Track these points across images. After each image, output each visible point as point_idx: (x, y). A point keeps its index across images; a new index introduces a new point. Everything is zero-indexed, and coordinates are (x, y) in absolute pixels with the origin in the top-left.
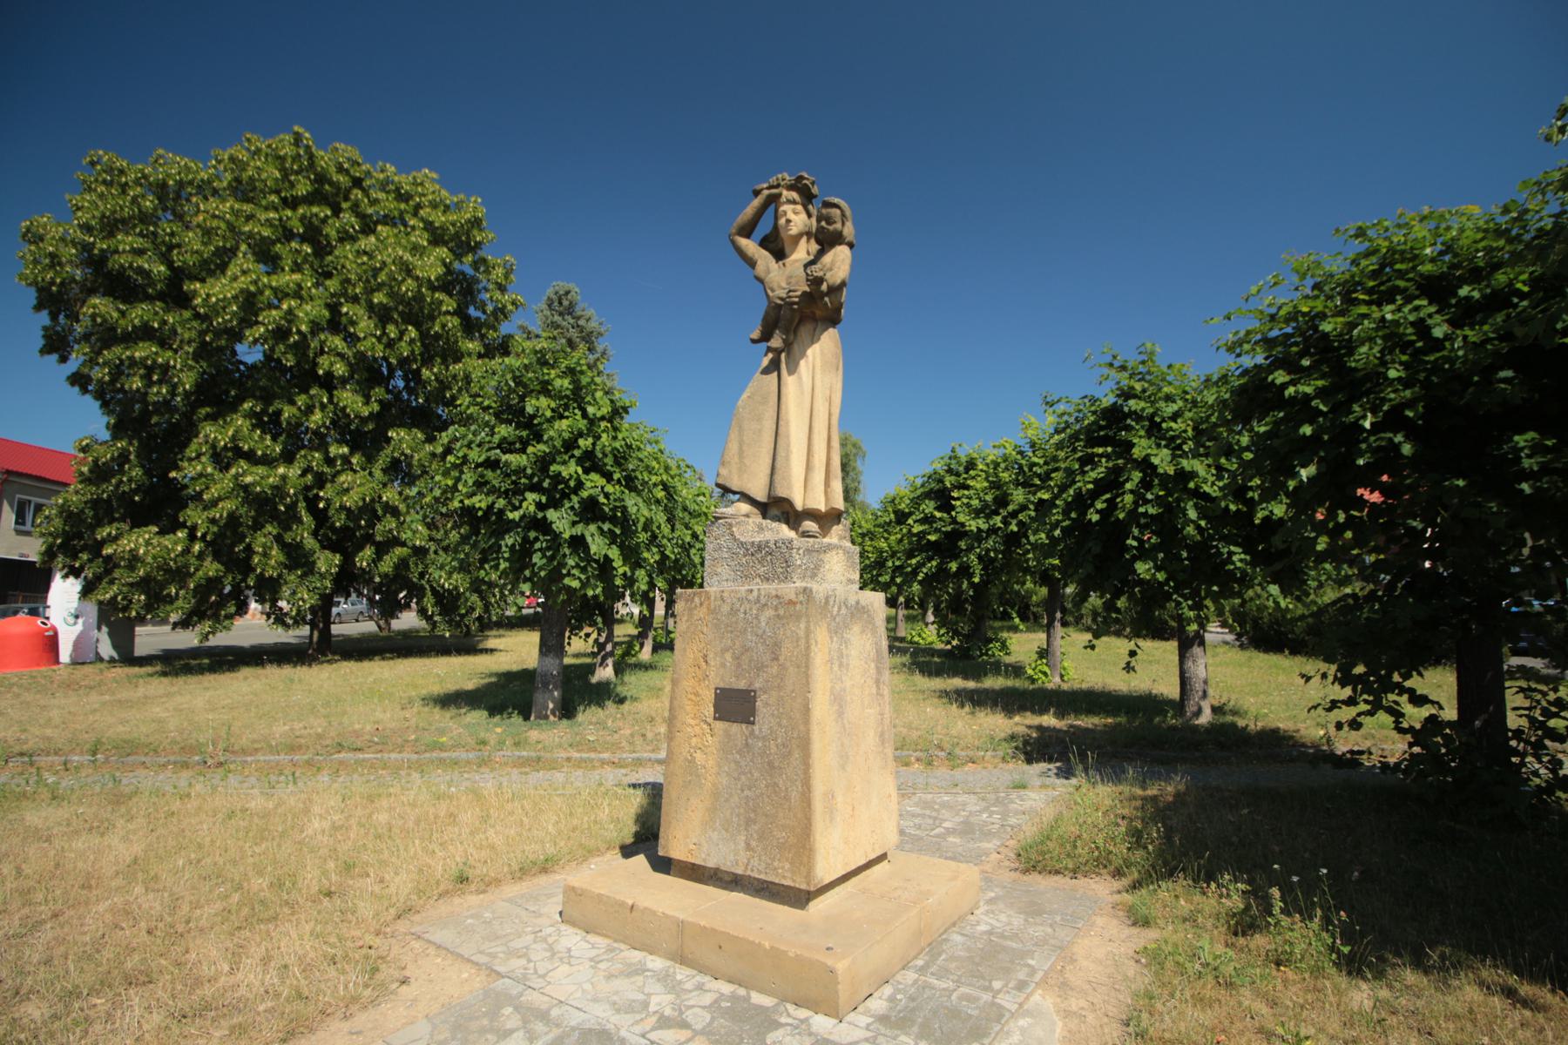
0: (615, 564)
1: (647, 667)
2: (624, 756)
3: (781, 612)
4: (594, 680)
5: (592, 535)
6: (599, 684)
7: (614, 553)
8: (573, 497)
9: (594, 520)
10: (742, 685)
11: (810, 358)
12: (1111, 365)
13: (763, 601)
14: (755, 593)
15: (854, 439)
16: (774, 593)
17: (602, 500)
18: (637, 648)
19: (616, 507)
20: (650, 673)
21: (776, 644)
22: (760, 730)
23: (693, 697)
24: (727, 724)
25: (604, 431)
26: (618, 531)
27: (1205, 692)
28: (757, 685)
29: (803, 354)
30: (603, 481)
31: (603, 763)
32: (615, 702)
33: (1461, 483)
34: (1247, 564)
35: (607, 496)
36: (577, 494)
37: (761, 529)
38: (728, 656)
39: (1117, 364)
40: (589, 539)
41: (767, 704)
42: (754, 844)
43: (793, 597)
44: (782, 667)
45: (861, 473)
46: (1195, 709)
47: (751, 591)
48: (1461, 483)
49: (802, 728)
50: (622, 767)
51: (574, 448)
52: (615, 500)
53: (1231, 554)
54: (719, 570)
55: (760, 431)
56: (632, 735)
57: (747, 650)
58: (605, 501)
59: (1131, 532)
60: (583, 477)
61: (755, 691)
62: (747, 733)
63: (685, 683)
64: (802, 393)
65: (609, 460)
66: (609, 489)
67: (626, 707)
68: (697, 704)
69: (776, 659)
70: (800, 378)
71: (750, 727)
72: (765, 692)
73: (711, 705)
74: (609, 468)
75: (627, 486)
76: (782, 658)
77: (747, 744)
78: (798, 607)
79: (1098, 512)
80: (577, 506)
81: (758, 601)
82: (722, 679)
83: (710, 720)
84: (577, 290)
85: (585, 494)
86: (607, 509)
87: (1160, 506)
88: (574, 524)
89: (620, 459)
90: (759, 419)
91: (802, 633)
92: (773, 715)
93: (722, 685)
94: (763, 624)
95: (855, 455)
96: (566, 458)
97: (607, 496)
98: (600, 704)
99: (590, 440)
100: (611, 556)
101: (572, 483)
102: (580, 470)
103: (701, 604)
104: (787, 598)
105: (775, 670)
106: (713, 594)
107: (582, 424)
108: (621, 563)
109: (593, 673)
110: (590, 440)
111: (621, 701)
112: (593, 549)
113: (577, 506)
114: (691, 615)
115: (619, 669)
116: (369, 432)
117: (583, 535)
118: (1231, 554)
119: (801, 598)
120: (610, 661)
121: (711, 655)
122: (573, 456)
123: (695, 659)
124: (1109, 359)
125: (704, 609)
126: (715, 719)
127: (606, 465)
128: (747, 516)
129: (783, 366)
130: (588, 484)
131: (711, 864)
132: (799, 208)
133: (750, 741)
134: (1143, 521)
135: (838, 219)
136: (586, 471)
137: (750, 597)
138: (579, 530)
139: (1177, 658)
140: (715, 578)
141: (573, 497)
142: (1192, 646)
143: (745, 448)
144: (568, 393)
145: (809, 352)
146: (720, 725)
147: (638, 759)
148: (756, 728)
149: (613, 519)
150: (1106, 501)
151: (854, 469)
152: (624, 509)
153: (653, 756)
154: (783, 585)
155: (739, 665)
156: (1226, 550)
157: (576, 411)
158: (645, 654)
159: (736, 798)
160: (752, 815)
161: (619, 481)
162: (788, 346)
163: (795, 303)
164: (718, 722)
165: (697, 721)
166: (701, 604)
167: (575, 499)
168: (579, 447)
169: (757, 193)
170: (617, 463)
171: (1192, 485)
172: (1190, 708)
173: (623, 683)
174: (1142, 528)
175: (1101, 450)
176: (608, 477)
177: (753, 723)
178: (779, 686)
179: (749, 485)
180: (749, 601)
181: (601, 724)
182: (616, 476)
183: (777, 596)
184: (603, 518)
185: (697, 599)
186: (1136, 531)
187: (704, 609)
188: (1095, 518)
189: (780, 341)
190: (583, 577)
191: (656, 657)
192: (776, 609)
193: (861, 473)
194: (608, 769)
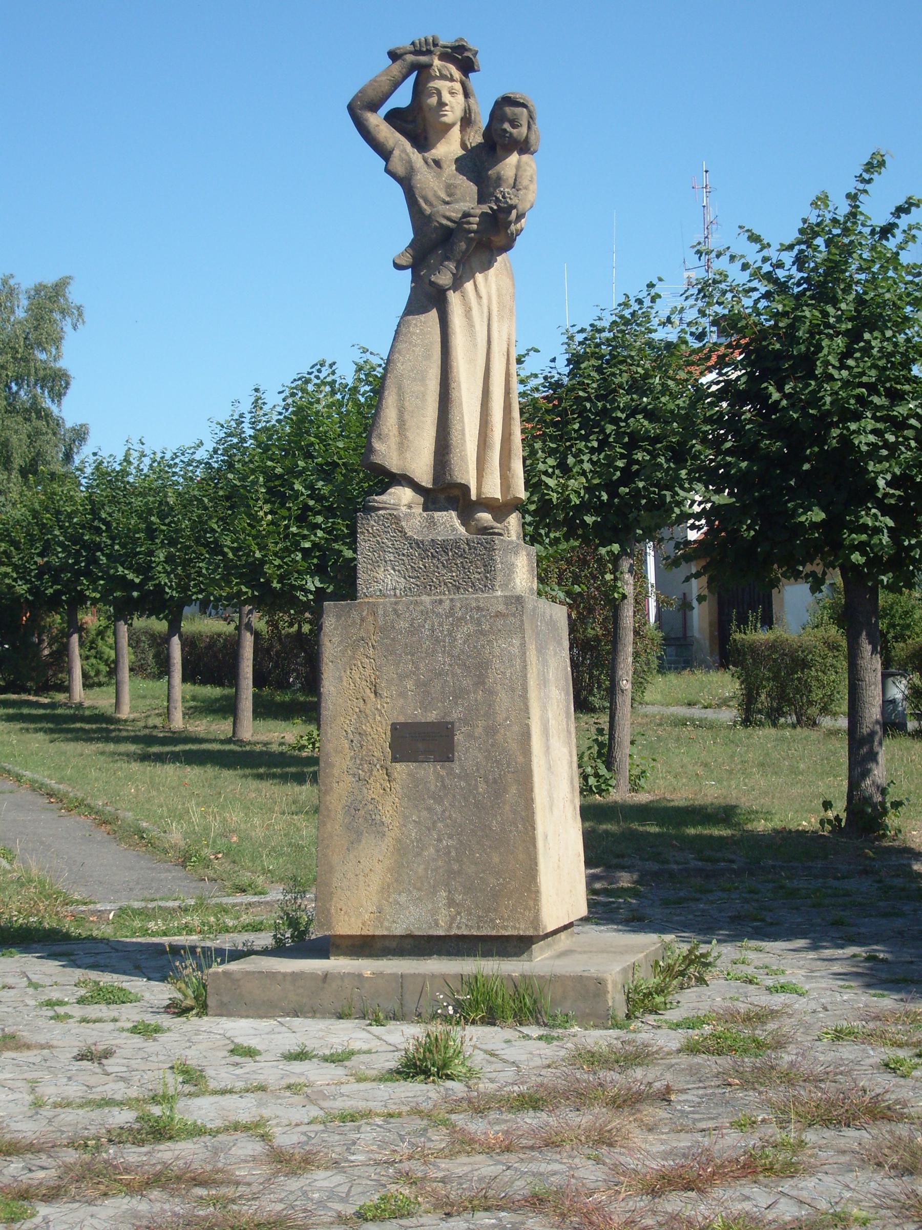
10: (432, 716)
24: (412, 766)
28: (455, 715)
33: (773, 417)
38: (410, 684)
42: (459, 898)
43: (501, 608)
44: (491, 692)
47: (441, 602)
48: (773, 417)
49: (520, 759)
61: (452, 723)
64: (475, 345)
90: (423, 380)
91: (515, 651)
93: (402, 719)
104: (493, 611)
116: (814, 526)
131: (399, 930)
135: (524, 122)
143: (406, 417)
146: (401, 769)
154: (480, 595)
159: (432, 850)
160: (456, 867)
164: (398, 765)
179: (414, 466)
180: (438, 615)
181: (258, 790)
189: (449, 275)
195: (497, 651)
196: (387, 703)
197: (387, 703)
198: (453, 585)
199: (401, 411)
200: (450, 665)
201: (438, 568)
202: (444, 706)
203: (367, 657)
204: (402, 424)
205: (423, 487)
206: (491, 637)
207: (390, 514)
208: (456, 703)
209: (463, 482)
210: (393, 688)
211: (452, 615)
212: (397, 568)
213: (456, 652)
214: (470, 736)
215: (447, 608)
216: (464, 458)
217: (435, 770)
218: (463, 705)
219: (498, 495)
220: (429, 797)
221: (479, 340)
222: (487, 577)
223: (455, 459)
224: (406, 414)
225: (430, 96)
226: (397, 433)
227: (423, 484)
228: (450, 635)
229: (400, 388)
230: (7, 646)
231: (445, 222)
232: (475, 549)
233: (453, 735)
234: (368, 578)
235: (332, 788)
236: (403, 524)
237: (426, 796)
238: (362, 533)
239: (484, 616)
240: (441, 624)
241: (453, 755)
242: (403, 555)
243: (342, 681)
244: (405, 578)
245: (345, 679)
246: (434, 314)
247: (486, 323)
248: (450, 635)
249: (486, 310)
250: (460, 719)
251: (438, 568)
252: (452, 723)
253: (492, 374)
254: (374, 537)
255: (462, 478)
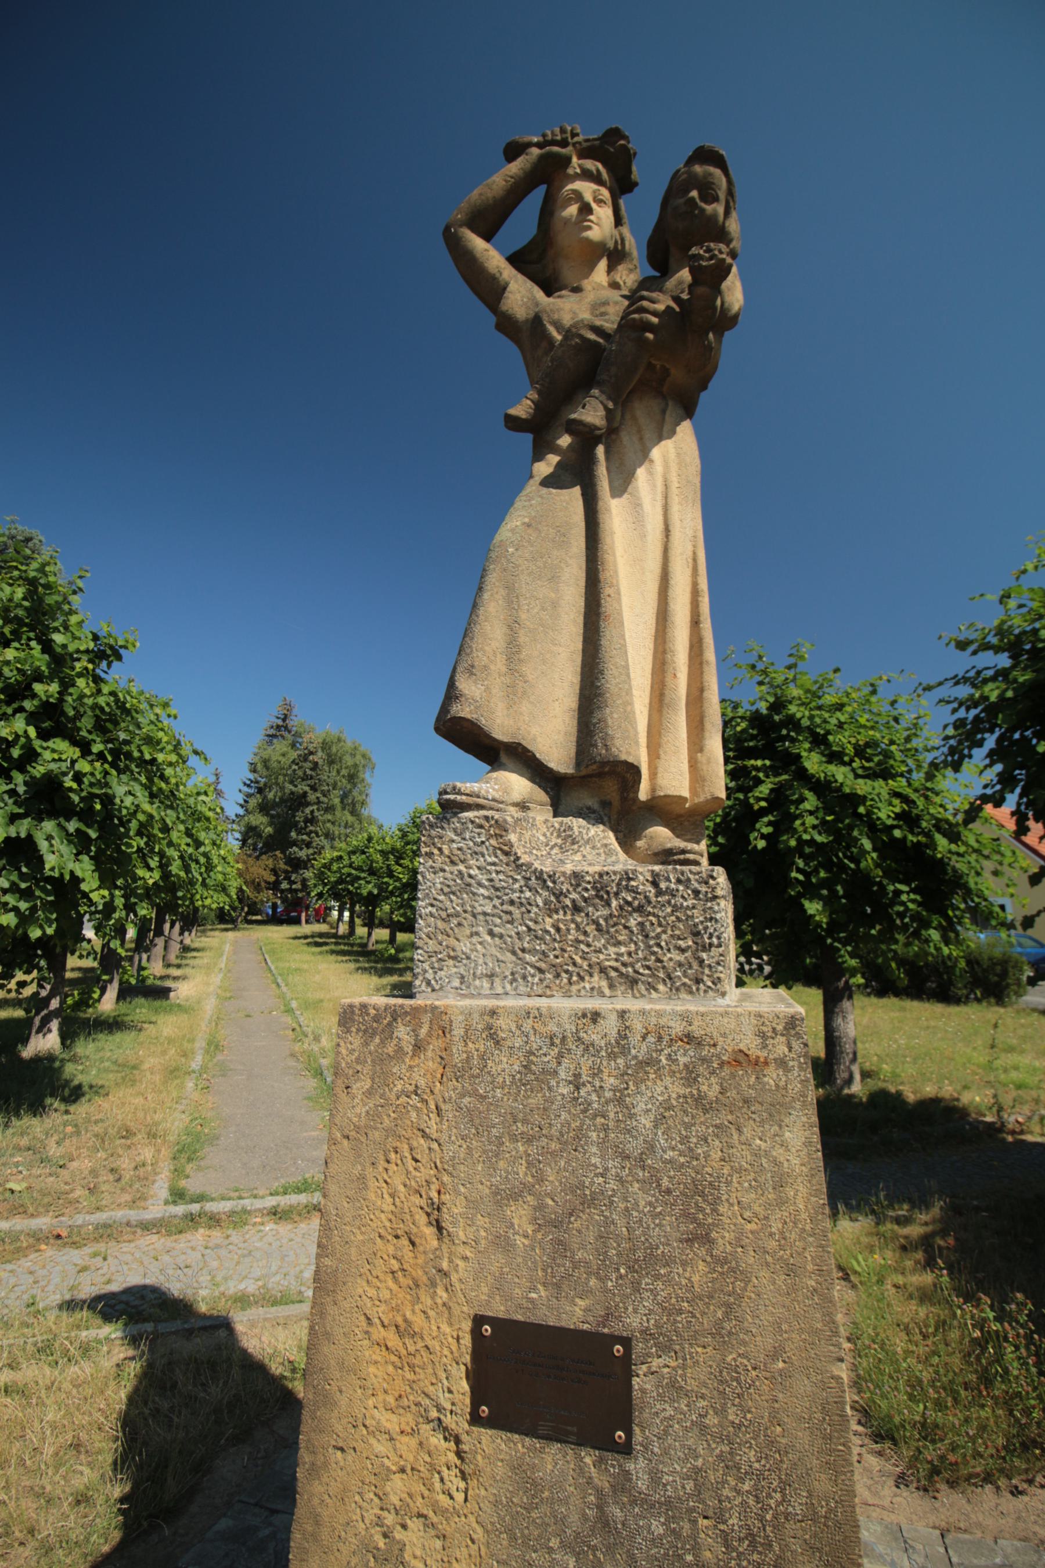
0: (84, 887)
1: (113, 1025)
2: (79, 1219)
3: (710, 1088)
4: (27, 1052)
5: (49, 838)
6: (37, 1060)
7: (85, 869)
8: (15, 774)
9: (52, 814)
11: (659, 468)
12: (753, 667)
13: (640, 1050)
14: (611, 1025)
15: (362, 749)
16: (678, 1028)
17: (69, 783)
18: (96, 996)
19: (92, 796)
20: (118, 1037)
21: (697, 1189)
22: (655, 1478)
23: (393, 1340)
24: (519, 1445)
25: (80, 675)
26: (93, 834)
27: (855, 1053)
28: (633, 1321)
29: (644, 456)
30: (75, 752)
31: (38, 1238)
32: (65, 1100)
34: (920, 904)
35: (78, 777)
36: (22, 770)
37: (569, 840)
38: (520, 1215)
39: (760, 666)
40: (43, 845)
41: (674, 1389)
43: (750, 1043)
45: (369, 785)
46: (846, 1075)
49: (822, 1484)
50: (75, 1245)
51: (24, 698)
52: (91, 785)
53: (898, 893)
54: (464, 946)
55: (555, 605)
56: (94, 1172)
57: (591, 1201)
58: (75, 786)
59: (793, 863)
60: (37, 744)
61: (627, 1342)
62: (603, 1482)
63: (361, 1287)
64: (643, 536)
65: (86, 723)
66: (83, 766)
67: (81, 1109)
68: (406, 1362)
69: (701, 1237)
70: (637, 505)
71: (613, 1460)
72: (665, 1348)
73: (459, 1372)
74: (84, 733)
75: (114, 765)
76: (723, 1239)
77: (604, 1522)
78: (772, 1076)
79: (763, 836)
80: (21, 789)
81: (621, 1045)
82: (499, 1286)
83: (459, 1423)
84: (41, 538)
85: (39, 770)
86: (76, 799)
87: (828, 832)
88: (13, 818)
89: (104, 724)
90: (554, 579)
92: (703, 1429)
93: (498, 1309)
94: (646, 1122)
95: (364, 766)
96: (9, 711)
97: (78, 777)
98: (37, 1108)
99: (54, 688)
100: (79, 873)
101: (16, 753)
102: (32, 732)
103: (418, 1047)
104: (727, 1046)
105: (699, 1275)
106: (458, 1020)
107: (40, 659)
108: (95, 884)
109: (25, 1041)
110: (54, 688)
111: (75, 1094)
112: (50, 861)
113: (21, 789)
114: (382, 1080)
115: (67, 1037)
117: (30, 837)
118: (898, 893)
119: (780, 1047)
120: (55, 1025)
121: (455, 1208)
122: (21, 709)
123: (398, 1215)
124: (753, 660)
125: (429, 1062)
126: (475, 1419)
127: (79, 729)
128: (523, 806)
129: (602, 470)
130: (47, 755)
132: (605, 193)
133: (616, 1512)
134: (807, 850)
136: (44, 735)
137: (593, 1035)
138: (23, 828)
139: (821, 1015)
140: (451, 968)
141: (15, 774)
142: (841, 1000)
143: (523, 638)
144: (21, 613)
145: (656, 453)
147: (106, 1226)
148: (638, 1467)
149: (86, 815)
150: (770, 823)
151: (363, 780)
152: (108, 800)
153: (133, 1215)
155: (561, 1247)
156: (891, 888)
157: (33, 643)
158: (108, 1003)
161: (101, 756)
162: (610, 434)
163: (648, 327)
164: (486, 1434)
165: (408, 1420)
166: (418, 1047)
167: (19, 778)
168: (34, 696)
169: (513, 151)
170: (100, 727)
171: (862, 810)
172: (841, 1075)
173: (74, 1059)
174: (807, 858)
175: (759, 763)
176: (85, 749)
177: (626, 1450)
178: (717, 1331)
179: (535, 730)
180: (588, 1047)
182: (96, 748)
183: (689, 1038)
184: (67, 811)
185: (402, 1032)
186: (801, 863)
187: (429, 1062)
188: (761, 844)
189: (602, 412)
190: (23, 906)
191: (123, 1007)
192: (690, 1077)
193: (369, 785)
194: (49, 1251)
195: (743, 1157)
196: (465, 1258)
197: (465, 1258)
198: (621, 974)
199: (513, 626)
200: (621, 1180)
201: (585, 933)
202: (606, 1290)
203: (425, 1135)
204: (513, 650)
205: (551, 770)
206: (725, 1117)
207: (487, 818)
208: (636, 1288)
209: (630, 760)
210: (480, 1220)
211: (625, 1051)
212: (496, 930)
213: (634, 1146)
214: (674, 1389)
215: (613, 1033)
216: (629, 717)
217: (581, 1470)
218: (654, 1292)
219: (686, 794)
220: (563, 1545)
221: (649, 527)
222: (701, 962)
223: (612, 716)
224: (522, 632)
225: (568, 202)
226: (504, 669)
227: (552, 765)
228: (620, 1101)
229: (510, 588)
230: (1019, 759)
231: (592, 336)
232: (673, 893)
233: (628, 1375)
234: (438, 948)
235: (326, 1464)
236: (513, 837)
237: (554, 1543)
238: (430, 855)
239: (703, 1060)
240: (596, 1073)
241: (629, 1434)
242: (512, 902)
243: (366, 1188)
244: (514, 953)
245: (372, 1184)
246: (577, 491)
247: (659, 497)
248: (620, 1101)
249: (660, 487)
250: (645, 1331)
251: (585, 933)
252: (627, 1342)
253: (672, 582)
254: (453, 862)
255: (628, 753)
